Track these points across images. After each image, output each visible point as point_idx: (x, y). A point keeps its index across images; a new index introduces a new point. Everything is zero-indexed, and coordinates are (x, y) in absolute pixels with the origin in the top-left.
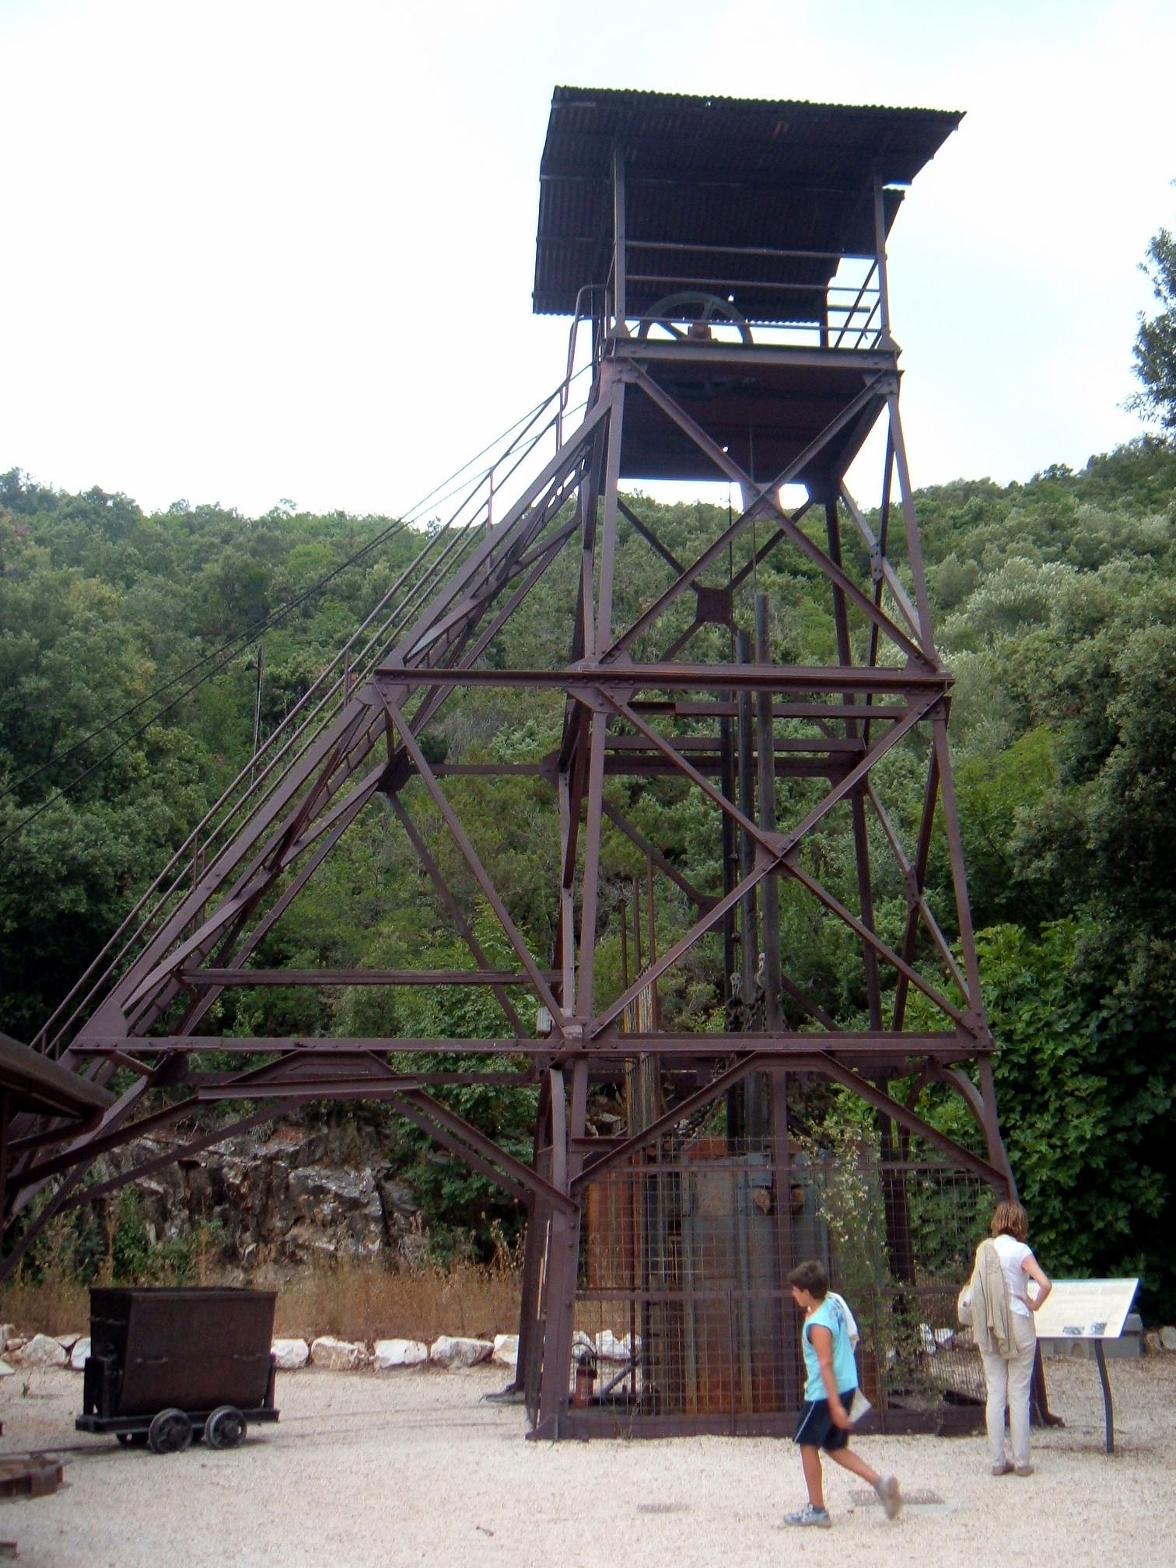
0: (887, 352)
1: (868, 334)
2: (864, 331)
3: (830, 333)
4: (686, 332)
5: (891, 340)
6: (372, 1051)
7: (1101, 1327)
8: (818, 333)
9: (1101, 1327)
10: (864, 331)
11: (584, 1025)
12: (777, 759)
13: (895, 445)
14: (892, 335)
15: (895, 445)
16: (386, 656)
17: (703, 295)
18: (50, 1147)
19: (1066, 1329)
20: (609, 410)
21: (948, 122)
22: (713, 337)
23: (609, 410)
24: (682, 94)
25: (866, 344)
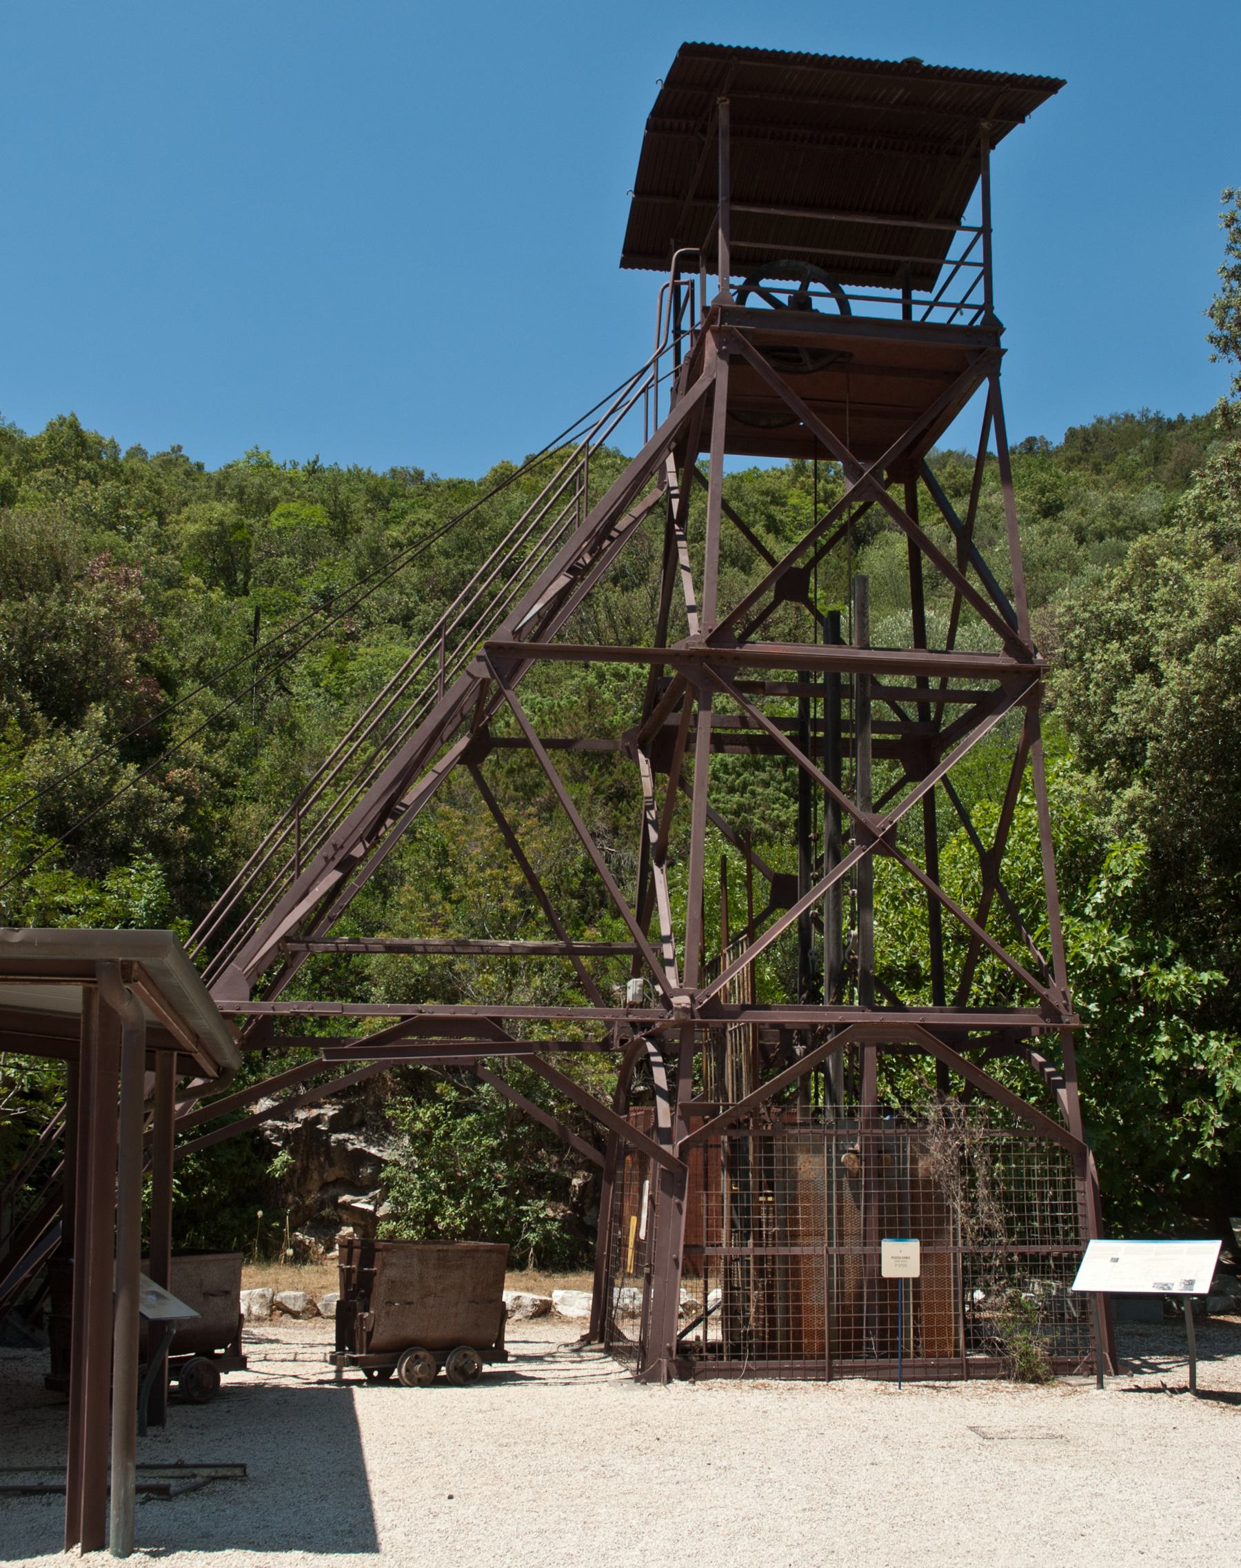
0: (993, 328)
1: (964, 310)
2: (959, 307)
3: (914, 307)
4: (786, 303)
5: (994, 317)
6: (491, 1018)
7: (1191, 1283)
8: (900, 306)
9: (1191, 1283)
10: (959, 307)
11: (692, 997)
12: (874, 741)
13: (994, 408)
14: (995, 312)
15: (994, 408)
16: (501, 622)
17: (802, 264)
18: (634, 646)
19: (1155, 1285)
20: (714, 382)
21: (1050, 86)
22: (814, 307)
23: (714, 382)
24: (787, 51)
25: (964, 319)
